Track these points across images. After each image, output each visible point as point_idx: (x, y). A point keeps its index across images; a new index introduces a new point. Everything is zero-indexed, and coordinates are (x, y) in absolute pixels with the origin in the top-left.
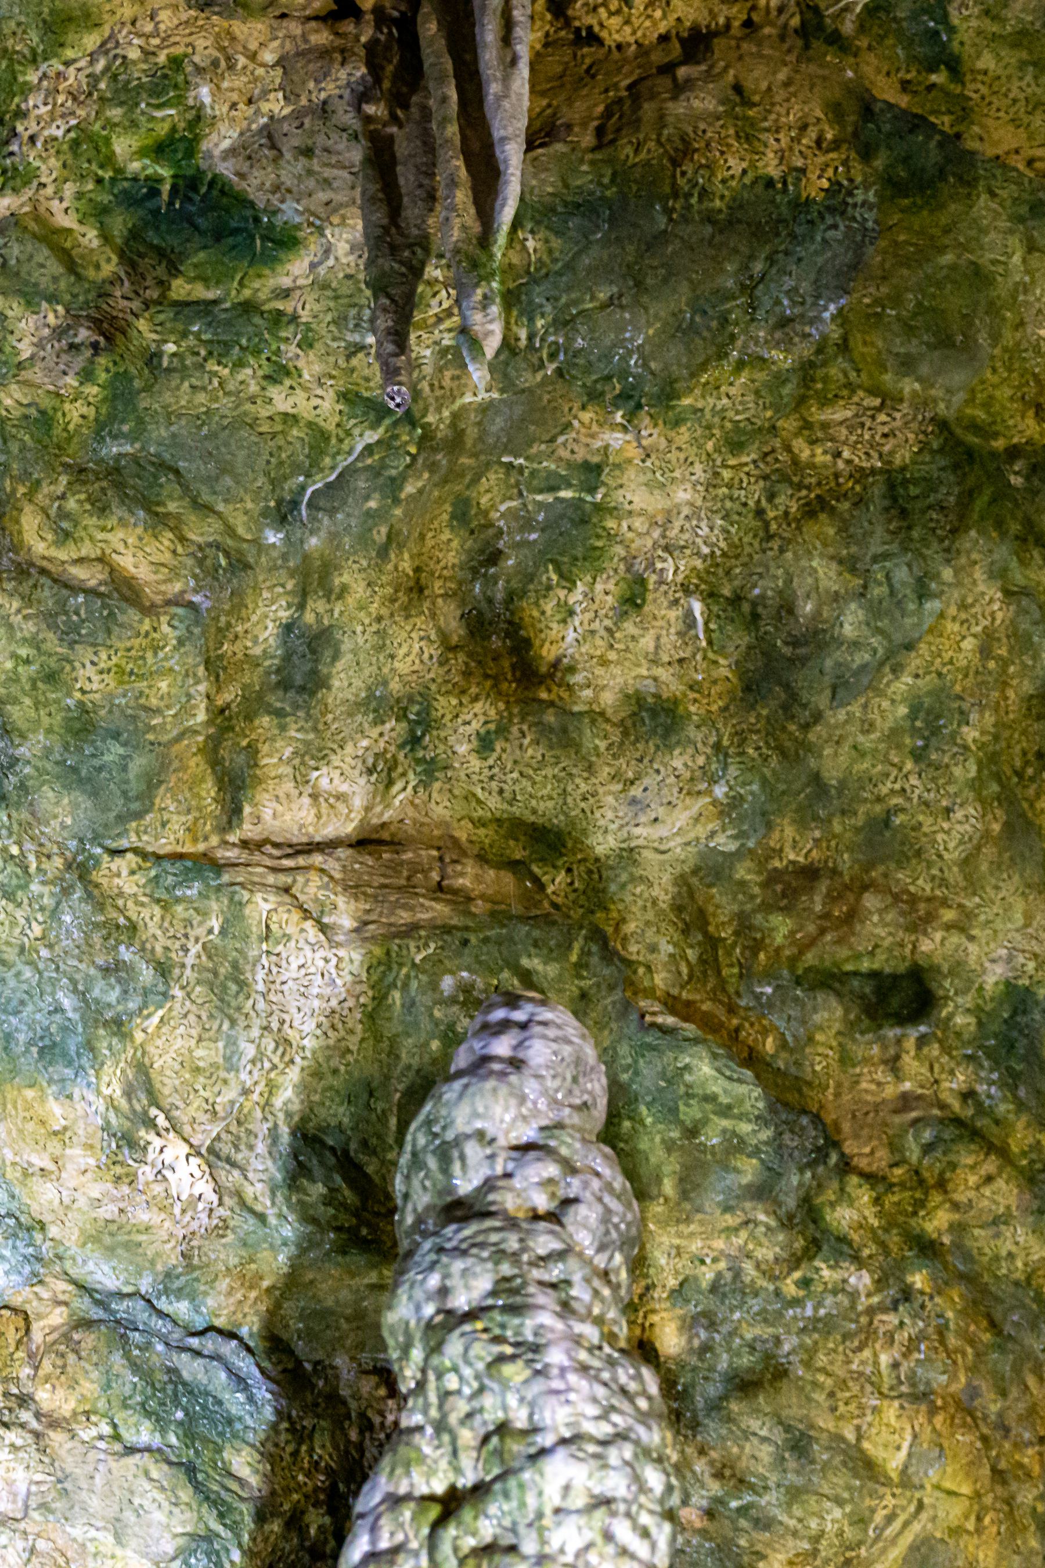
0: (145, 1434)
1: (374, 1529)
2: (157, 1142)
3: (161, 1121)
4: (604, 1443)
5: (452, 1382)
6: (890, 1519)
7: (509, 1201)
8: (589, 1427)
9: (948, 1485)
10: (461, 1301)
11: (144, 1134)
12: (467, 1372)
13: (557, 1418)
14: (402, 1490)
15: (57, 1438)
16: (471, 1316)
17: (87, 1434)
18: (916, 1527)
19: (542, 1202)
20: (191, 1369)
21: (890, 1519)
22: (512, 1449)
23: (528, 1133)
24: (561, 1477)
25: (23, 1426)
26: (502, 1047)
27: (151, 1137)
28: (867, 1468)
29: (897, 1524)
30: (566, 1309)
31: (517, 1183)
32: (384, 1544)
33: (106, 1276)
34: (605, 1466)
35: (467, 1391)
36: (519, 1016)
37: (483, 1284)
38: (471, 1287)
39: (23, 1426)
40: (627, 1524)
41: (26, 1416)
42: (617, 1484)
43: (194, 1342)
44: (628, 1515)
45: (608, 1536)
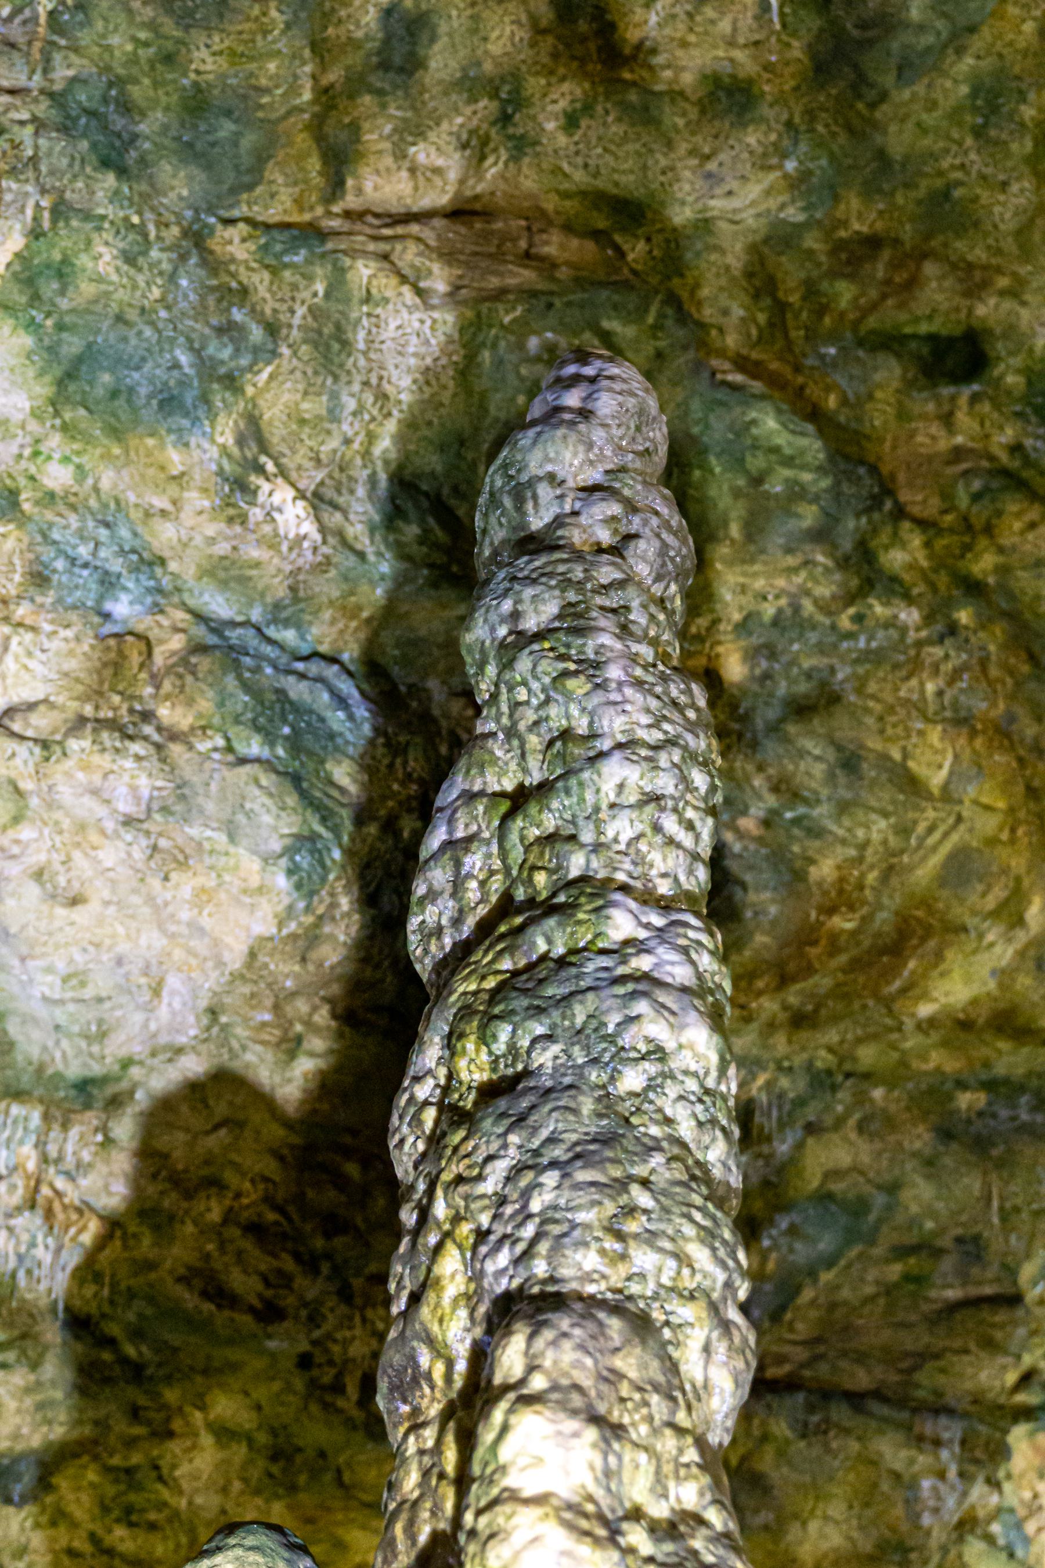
0: (255, 747)
1: (451, 822)
2: (266, 487)
3: (270, 467)
4: (655, 748)
5: (522, 694)
6: (931, 830)
7: (576, 537)
8: (642, 734)
9: (985, 800)
10: (531, 623)
11: (255, 479)
12: (535, 686)
13: (614, 725)
14: (476, 788)
15: (176, 749)
16: (539, 636)
17: (203, 746)
18: (955, 838)
19: (605, 536)
20: (297, 690)
21: (931, 830)
22: (574, 753)
23: (594, 476)
24: (616, 775)
25: (146, 738)
26: (572, 399)
27: (261, 481)
28: (911, 785)
29: (937, 835)
30: (625, 631)
31: (583, 519)
32: (460, 834)
33: (220, 605)
34: (657, 768)
35: (535, 702)
36: (589, 371)
37: (551, 608)
38: (541, 610)
39: (146, 738)
40: (674, 817)
41: (148, 730)
42: (666, 783)
43: (300, 666)
44: (675, 810)
45: (657, 828)
